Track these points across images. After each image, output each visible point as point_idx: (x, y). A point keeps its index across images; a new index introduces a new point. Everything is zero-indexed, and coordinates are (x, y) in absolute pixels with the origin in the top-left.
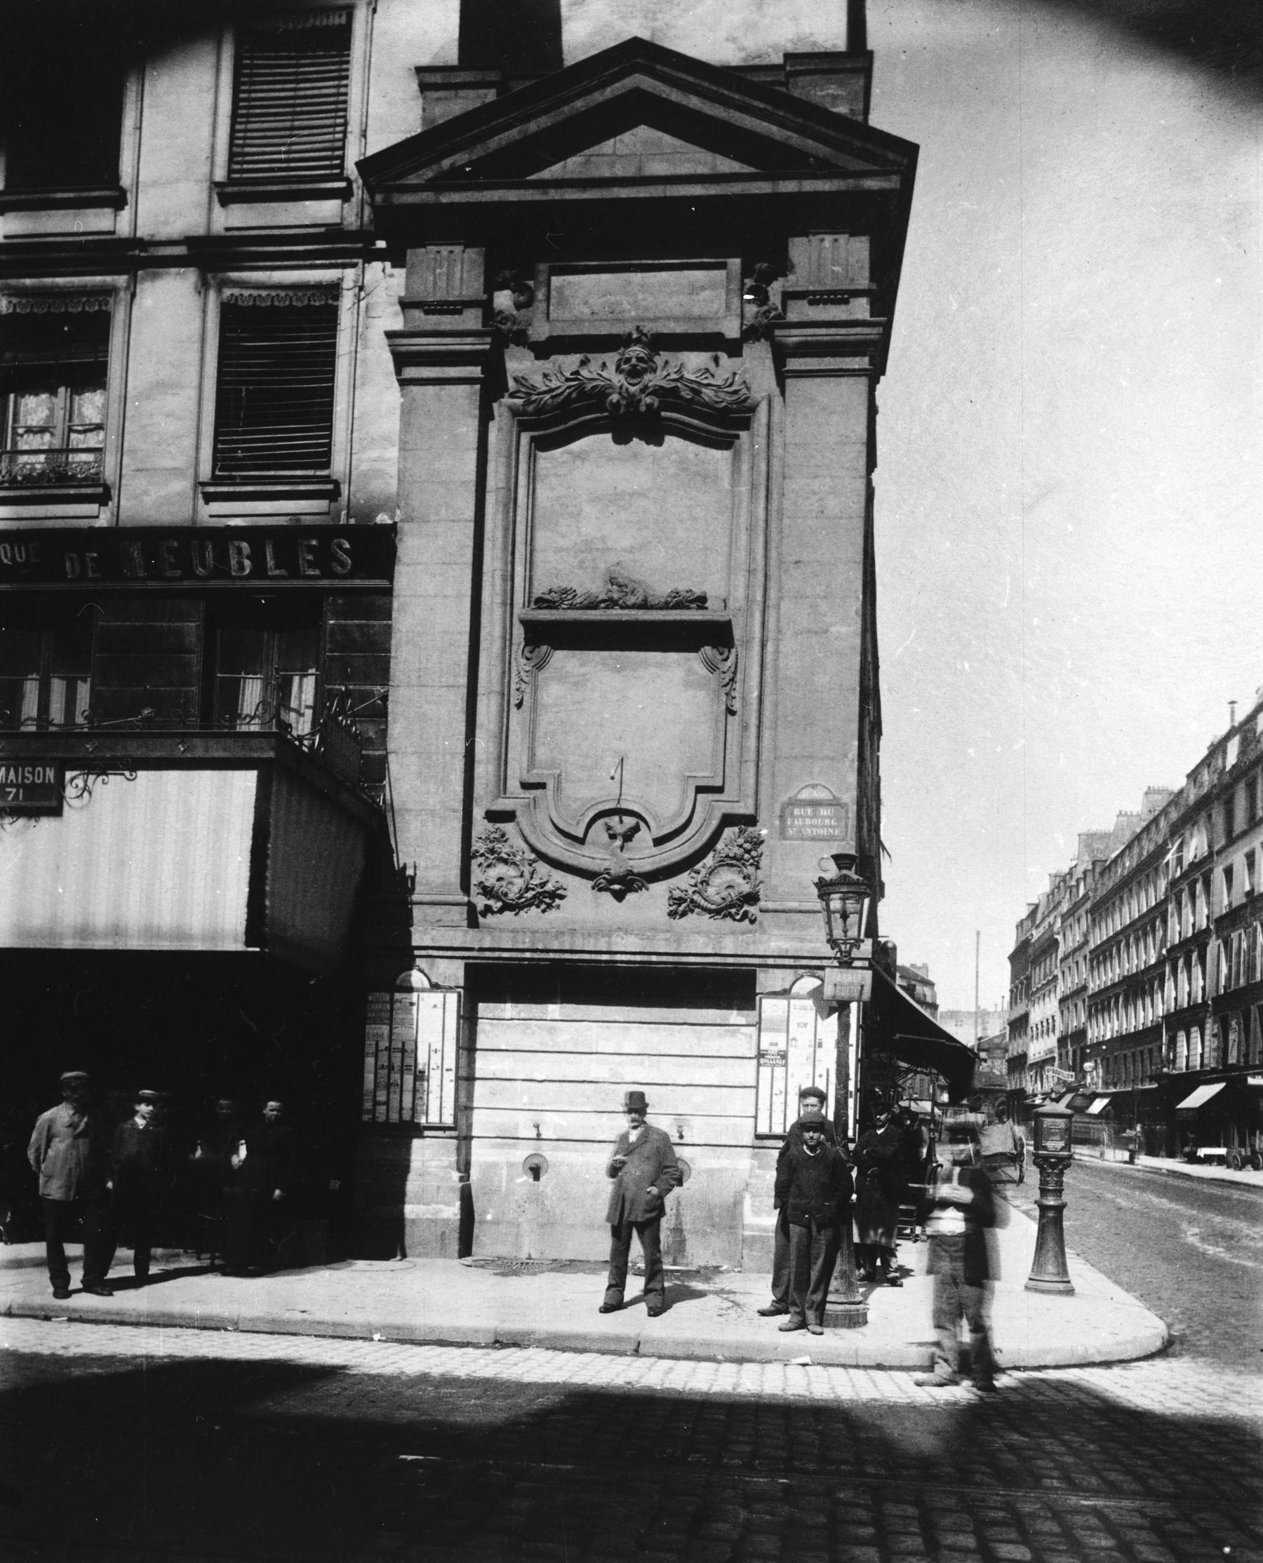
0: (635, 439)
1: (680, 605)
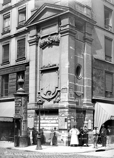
1: (53, 66)
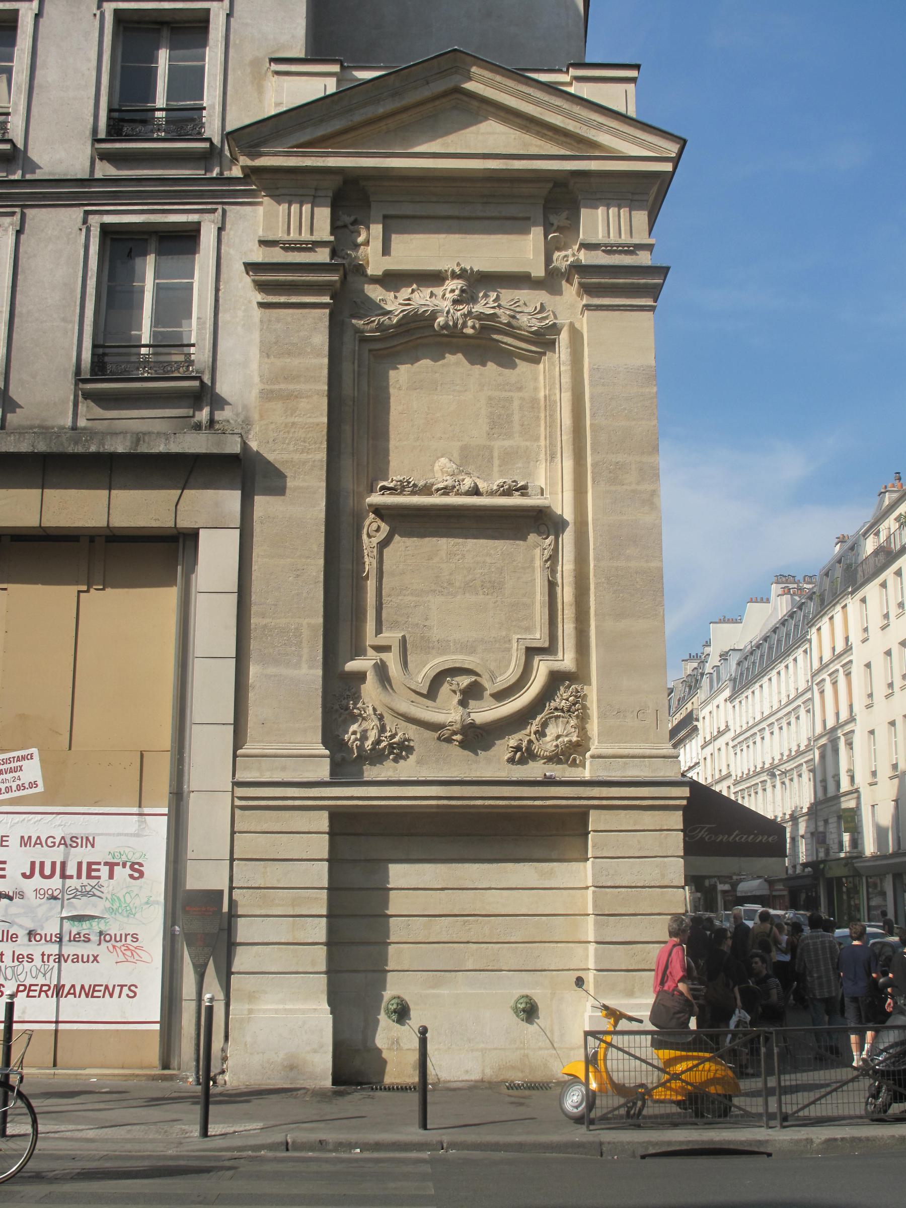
0: (447, 355)
